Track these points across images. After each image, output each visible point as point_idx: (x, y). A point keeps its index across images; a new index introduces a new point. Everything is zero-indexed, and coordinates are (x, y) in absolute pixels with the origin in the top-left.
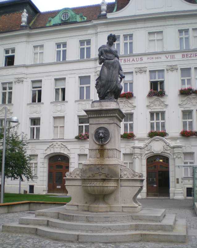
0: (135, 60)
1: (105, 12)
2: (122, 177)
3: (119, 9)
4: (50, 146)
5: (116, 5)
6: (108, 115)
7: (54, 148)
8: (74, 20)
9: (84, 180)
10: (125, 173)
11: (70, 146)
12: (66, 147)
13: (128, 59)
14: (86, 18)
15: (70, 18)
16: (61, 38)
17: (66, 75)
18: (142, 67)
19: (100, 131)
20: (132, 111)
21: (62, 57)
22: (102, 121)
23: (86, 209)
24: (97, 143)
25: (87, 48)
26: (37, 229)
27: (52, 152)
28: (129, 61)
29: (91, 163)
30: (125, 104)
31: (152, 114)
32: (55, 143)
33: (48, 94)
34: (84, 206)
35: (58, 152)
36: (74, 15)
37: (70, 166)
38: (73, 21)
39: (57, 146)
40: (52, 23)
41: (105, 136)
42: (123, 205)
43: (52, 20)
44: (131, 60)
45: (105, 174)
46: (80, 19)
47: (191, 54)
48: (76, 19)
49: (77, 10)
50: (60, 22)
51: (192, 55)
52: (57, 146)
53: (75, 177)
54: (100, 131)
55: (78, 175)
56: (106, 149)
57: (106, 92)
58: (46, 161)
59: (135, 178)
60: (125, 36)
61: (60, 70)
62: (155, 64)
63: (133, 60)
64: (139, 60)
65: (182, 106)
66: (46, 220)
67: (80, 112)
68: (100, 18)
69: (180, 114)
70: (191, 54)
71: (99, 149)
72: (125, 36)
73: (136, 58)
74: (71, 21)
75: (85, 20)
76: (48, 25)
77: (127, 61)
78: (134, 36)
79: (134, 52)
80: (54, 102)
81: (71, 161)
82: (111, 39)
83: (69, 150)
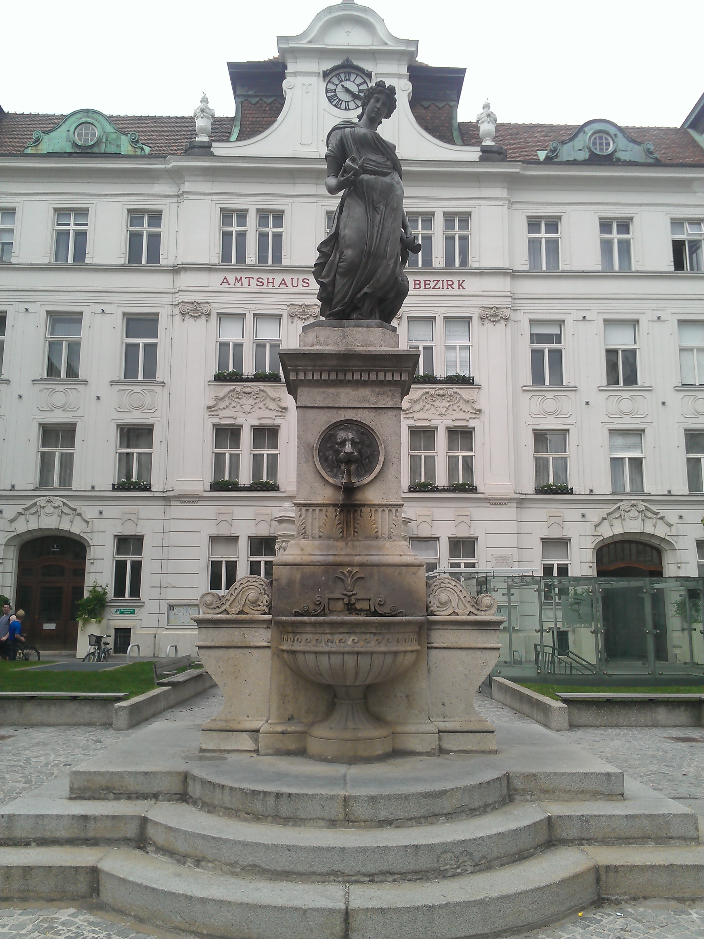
0: (289, 283)
1: (206, 139)
2: (432, 614)
3: (243, 136)
4: (26, 509)
5: (238, 123)
6: (373, 377)
7: (39, 516)
8: (112, 149)
9: (284, 629)
10: (444, 597)
11: (90, 511)
12: (79, 514)
13: (268, 279)
14: (147, 150)
15: (101, 141)
16: (72, 194)
17: (87, 304)
18: (498, 306)
19: (342, 435)
20: (277, 421)
21: (71, 249)
22: (347, 396)
23: (292, 746)
24: (331, 480)
25: (150, 235)
26: (94, 872)
27: (33, 525)
28: (270, 285)
29: (307, 559)
30: (257, 401)
31: (682, 350)
32: (42, 502)
33: (584, 357)
34: (283, 733)
35: (53, 527)
36: (114, 136)
37: (88, 568)
38: (108, 150)
39: (49, 509)
40: (44, 147)
41: (361, 456)
42: (443, 726)
43: (46, 138)
44: (277, 282)
45: (369, 600)
46: (130, 148)
47: (438, 281)
48: (118, 146)
49: (124, 124)
50: (69, 150)
51: (440, 285)
52: (49, 509)
53: (241, 612)
54: (342, 435)
55: (254, 603)
56: (364, 505)
57: (359, 295)
58: (12, 554)
59: (482, 617)
60: (263, 216)
61: (67, 288)
62: (537, 209)
63: (283, 282)
64: (300, 285)
65: (411, 415)
66: (132, 817)
67: (123, 415)
68: (190, 151)
69: (210, 435)
70: (438, 281)
71: (335, 505)
72: (263, 216)
73: (292, 279)
74: (103, 151)
75: (147, 153)
76: (29, 151)
77: (265, 284)
78: (286, 220)
79: (285, 262)
80: (45, 380)
81: (91, 554)
82: (378, 100)
83: (87, 522)
